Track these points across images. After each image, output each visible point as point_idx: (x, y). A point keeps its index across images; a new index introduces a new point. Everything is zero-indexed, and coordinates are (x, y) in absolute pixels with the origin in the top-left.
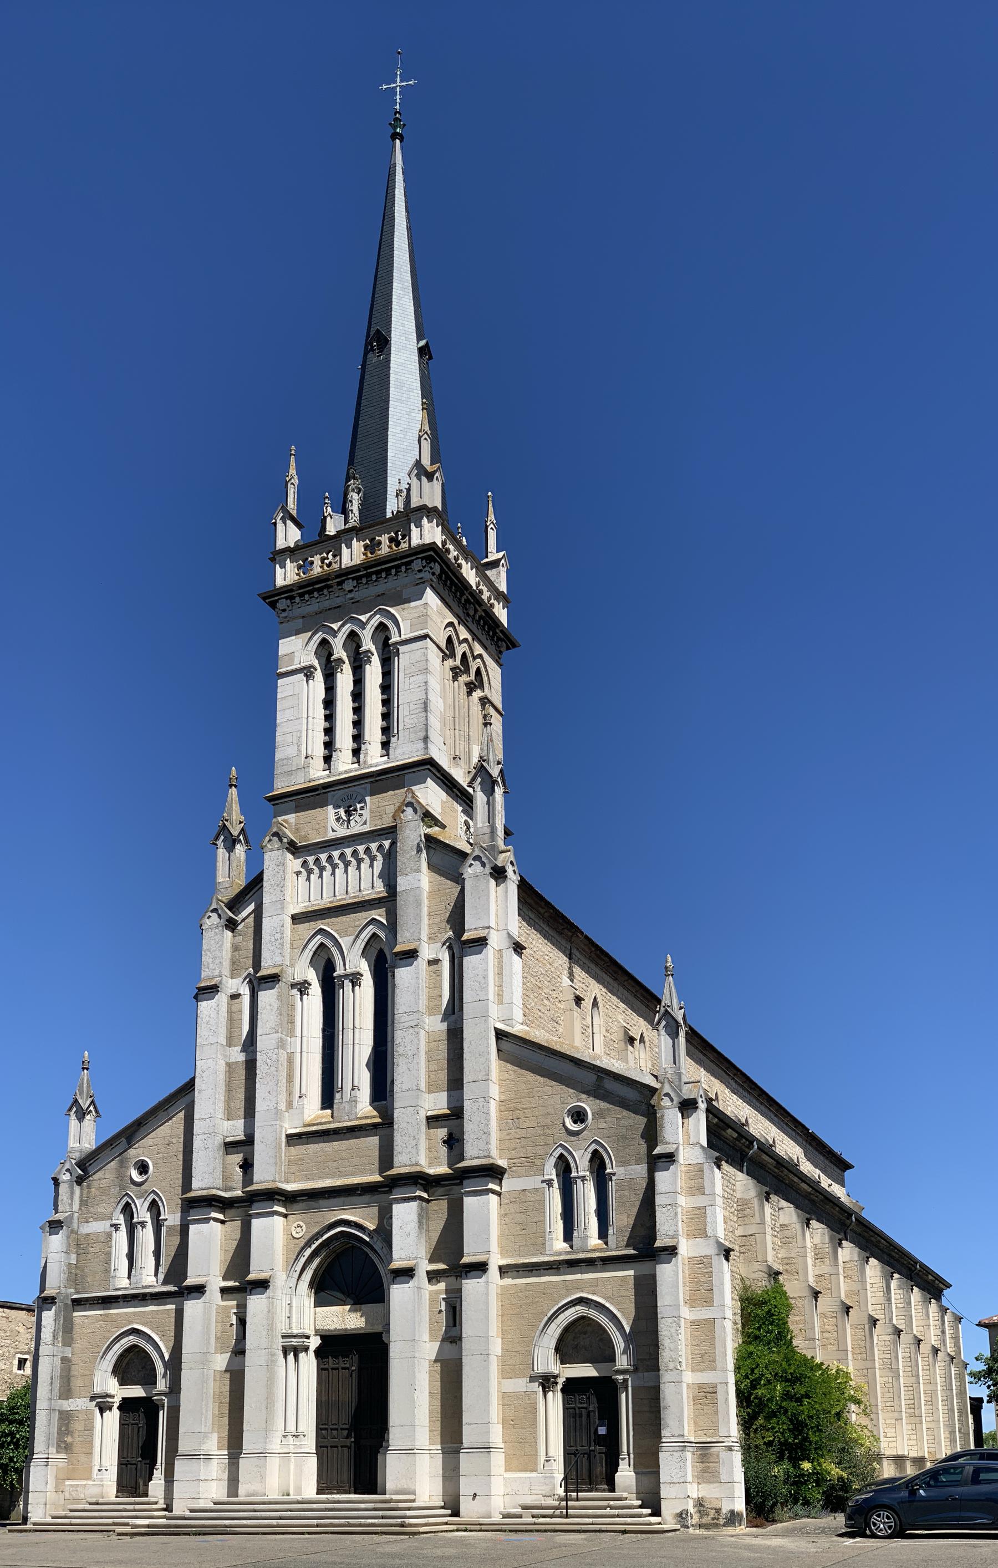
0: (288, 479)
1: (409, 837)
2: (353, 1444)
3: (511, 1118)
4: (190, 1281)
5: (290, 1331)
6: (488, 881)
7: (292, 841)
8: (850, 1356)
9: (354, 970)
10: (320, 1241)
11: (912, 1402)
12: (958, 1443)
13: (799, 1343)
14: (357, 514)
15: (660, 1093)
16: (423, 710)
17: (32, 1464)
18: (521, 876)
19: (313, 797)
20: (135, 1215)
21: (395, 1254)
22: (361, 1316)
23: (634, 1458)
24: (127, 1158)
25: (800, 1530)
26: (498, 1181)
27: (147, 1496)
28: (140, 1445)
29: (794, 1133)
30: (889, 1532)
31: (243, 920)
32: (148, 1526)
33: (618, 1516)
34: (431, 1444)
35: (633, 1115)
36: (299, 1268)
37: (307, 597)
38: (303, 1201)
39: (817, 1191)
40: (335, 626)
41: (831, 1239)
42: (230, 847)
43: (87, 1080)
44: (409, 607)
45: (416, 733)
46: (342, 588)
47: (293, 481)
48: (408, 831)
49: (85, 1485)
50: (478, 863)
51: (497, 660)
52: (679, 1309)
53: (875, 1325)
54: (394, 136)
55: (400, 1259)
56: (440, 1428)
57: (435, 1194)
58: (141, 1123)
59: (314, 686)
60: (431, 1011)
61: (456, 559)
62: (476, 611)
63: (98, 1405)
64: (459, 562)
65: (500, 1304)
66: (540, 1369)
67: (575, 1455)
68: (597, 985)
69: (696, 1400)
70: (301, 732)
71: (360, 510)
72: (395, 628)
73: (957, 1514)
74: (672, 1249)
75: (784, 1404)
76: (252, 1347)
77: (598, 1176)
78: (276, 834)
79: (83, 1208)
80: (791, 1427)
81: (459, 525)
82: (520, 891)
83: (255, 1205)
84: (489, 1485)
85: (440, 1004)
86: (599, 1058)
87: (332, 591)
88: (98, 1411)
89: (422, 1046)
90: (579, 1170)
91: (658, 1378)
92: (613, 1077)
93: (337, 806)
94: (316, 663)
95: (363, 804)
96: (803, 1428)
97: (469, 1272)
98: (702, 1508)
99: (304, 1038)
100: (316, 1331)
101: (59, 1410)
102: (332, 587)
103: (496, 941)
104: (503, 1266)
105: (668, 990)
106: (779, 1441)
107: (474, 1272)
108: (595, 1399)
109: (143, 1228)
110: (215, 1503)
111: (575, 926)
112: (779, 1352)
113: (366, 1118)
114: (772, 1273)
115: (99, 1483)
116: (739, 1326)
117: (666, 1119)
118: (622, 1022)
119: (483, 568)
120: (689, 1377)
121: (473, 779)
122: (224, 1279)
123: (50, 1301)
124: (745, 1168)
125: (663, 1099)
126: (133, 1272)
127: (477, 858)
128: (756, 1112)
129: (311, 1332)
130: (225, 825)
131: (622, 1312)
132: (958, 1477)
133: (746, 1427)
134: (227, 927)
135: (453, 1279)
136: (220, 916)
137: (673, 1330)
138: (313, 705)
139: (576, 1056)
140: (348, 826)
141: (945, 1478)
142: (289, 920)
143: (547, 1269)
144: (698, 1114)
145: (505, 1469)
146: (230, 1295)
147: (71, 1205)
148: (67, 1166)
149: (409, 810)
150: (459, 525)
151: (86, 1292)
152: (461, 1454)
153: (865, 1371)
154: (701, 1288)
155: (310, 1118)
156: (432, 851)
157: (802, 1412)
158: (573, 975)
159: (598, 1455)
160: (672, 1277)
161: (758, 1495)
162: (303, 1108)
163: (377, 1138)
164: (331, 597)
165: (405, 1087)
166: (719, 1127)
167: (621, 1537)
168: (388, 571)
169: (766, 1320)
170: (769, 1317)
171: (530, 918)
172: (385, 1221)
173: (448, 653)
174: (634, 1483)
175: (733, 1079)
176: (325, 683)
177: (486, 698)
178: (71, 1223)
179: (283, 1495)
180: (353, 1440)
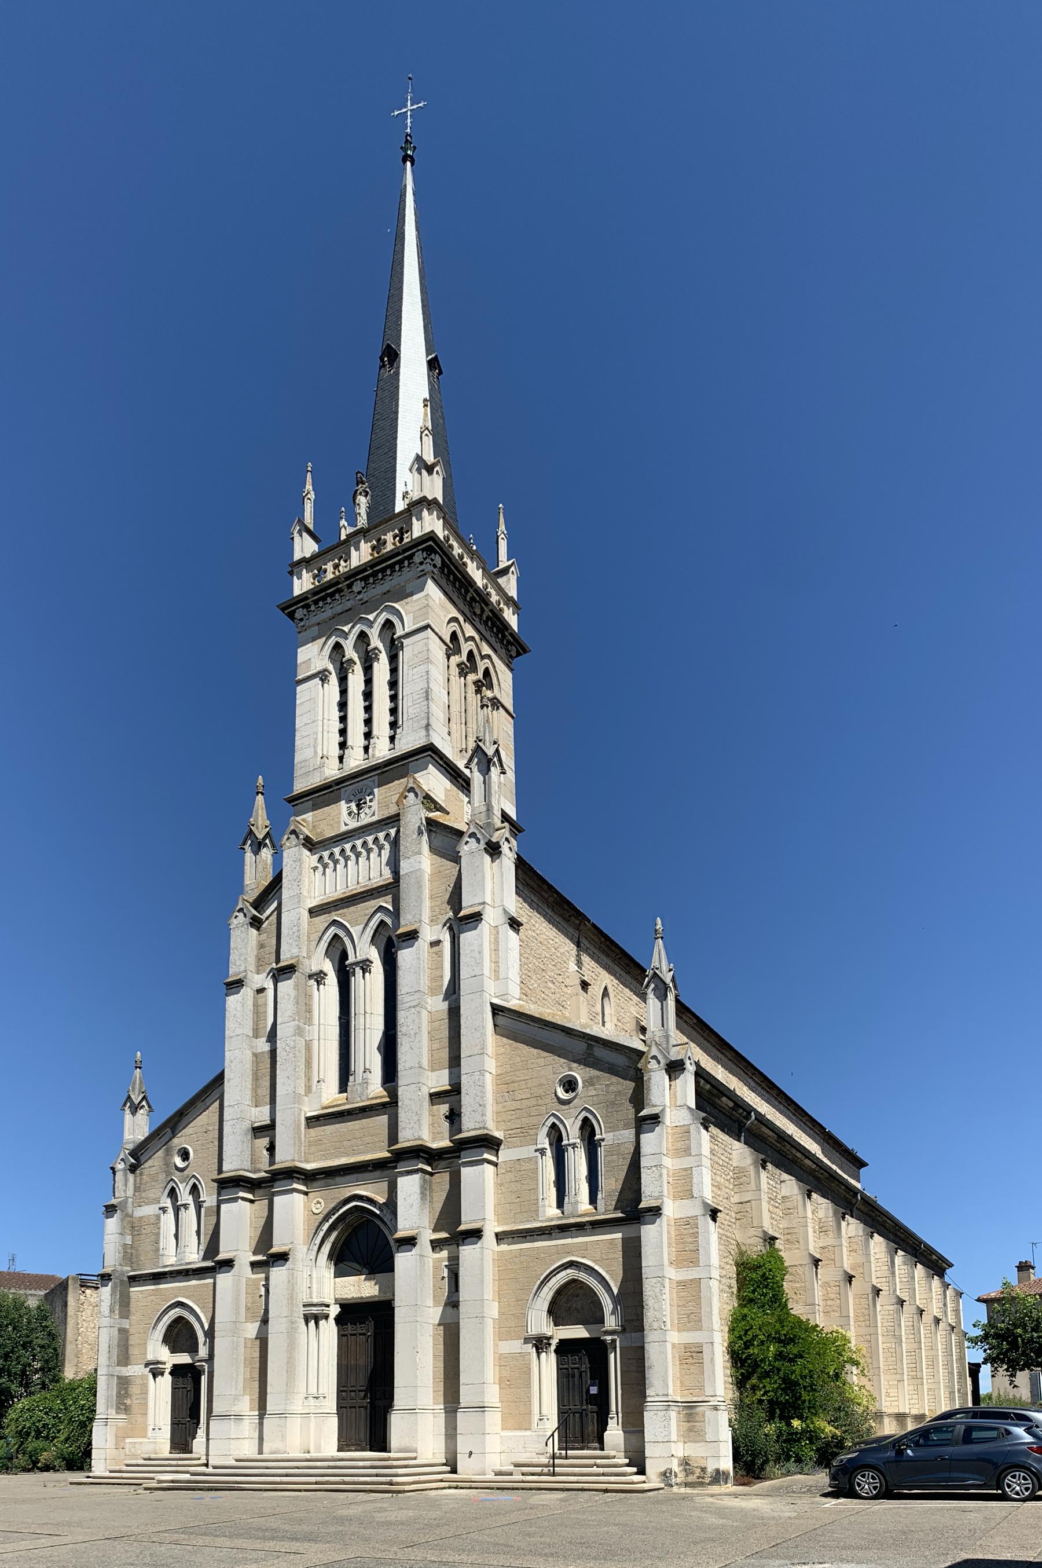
0: (304, 494)
2: (369, 1405)
3: (507, 1090)
4: (221, 1257)
5: (310, 1300)
7: (307, 836)
8: (852, 1323)
9: (364, 957)
10: (337, 1215)
11: (915, 1365)
12: (957, 1401)
13: (797, 1309)
14: (365, 517)
15: (647, 1056)
16: (424, 699)
17: (94, 1424)
18: (517, 854)
20: (179, 1199)
21: (400, 1226)
22: (375, 1284)
23: (623, 1417)
25: (787, 1488)
26: (495, 1152)
28: (189, 1407)
29: (812, 1132)
30: (874, 1492)
31: (267, 918)
32: (173, 1481)
33: (603, 1475)
35: (622, 1080)
36: (318, 1241)
37: (321, 604)
38: (322, 1178)
39: (821, 1168)
40: (346, 629)
41: (835, 1213)
42: (256, 852)
43: (140, 1078)
45: (418, 721)
46: (352, 591)
47: (309, 496)
48: (410, 816)
49: (141, 1443)
50: (473, 840)
51: (507, 664)
52: (663, 1270)
53: (878, 1295)
56: (442, 1389)
57: (439, 1168)
58: (183, 1114)
59: (329, 689)
60: (433, 992)
61: (461, 557)
62: (483, 611)
63: (151, 1371)
64: (464, 560)
65: (497, 1269)
68: (607, 975)
70: (317, 735)
71: (368, 514)
72: (400, 623)
73: (947, 1475)
74: (658, 1209)
78: (293, 832)
79: (136, 1194)
81: (471, 536)
82: (520, 871)
83: (278, 1183)
84: (483, 1443)
85: (441, 984)
87: (344, 595)
92: (603, 1044)
93: (349, 801)
94: (331, 668)
95: (372, 797)
97: (466, 1238)
98: (688, 1467)
100: (336, 1300)
101: (117, 1376)
103: (492, 917)
105: (657, 953)
107: (470, 1239)
108: (587, 1360)
109: (186, 1209)
110: (237, 1460)
111: (582, 913)
112: (773, 1314)
113: (376, 1098)
114: (767, 1238)
116: (735, 1290)
117: (653, 1081)
118: (635, 1013)
119: (489, 561)
120: (674, 1337)
121: (470, 760)
122: (255, 1253)
124: (742, 1138)
125: (650, 1062)
127: (473, 835)
128: (774, 1110)
130: (251, 829)
131: (610, 1274)
132: (949, 1436)
134: (252, 925)
136: (245, 915)
137: (657, 1290)
138: (329, 708)
139: (567, 1025)
140: (358, 819)
141: (936, 1437)
142: (306, 914)
143: (540, 1235)
144: (685, 1076)
146: (260, 1268)
147: (125, 1191)
148: (122, 1156)
149: (411, 795)
150: (471, 536)
151: (140, 1270)
153: (868, 1337)
154: (687, 1249)
155: (328, 1102)
157: (794, 1372)
158: (581, 963)
159: (590, 1414)
161: (747, 1454)
162: (321, 1092)
163: (386, 1117)
164: (343, 601)
165: (408, 1066)
168: (392, 567)
169: (761, 1283)
171: (532, 901)
173: (452, 646)
175: (751, 1078)
176: (340, 686)
177: (495, 698)
178: (126, 1207)
179: (304, 1453)
180: (369, 1400)
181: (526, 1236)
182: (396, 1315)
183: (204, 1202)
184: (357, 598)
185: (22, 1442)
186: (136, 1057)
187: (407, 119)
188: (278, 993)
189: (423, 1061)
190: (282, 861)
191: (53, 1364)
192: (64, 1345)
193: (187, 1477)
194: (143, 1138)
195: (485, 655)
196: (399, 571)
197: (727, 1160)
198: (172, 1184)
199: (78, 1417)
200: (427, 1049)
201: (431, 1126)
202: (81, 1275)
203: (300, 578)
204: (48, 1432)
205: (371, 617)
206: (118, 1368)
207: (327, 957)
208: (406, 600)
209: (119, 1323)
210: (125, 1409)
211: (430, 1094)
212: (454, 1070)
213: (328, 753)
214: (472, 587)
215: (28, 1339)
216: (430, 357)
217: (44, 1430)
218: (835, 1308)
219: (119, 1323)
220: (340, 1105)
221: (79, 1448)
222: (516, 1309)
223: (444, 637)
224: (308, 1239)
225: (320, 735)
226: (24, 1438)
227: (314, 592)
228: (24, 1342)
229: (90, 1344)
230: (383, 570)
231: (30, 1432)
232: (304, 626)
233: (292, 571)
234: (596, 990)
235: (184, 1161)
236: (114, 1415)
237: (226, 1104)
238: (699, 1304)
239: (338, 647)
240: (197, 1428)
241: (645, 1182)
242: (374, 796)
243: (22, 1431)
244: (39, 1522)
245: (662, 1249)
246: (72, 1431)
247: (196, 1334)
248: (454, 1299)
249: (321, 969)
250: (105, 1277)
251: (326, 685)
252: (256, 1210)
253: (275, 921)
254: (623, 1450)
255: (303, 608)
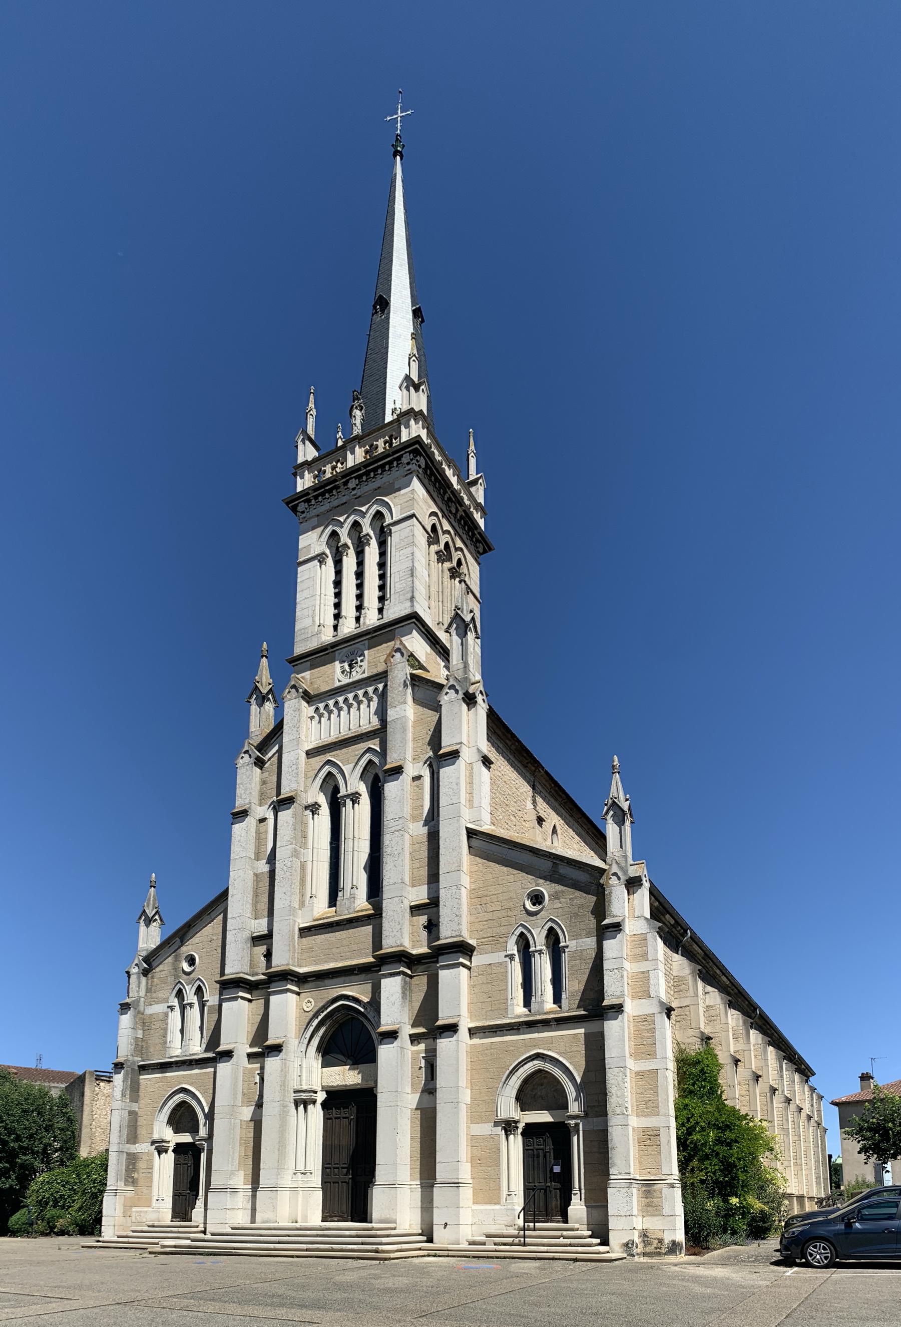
1: (397, 676)
2: (350, 1180)
4: (222, 1048)
5: (300, 1087)
6: (461, 705)
7: (306, 690)
9: (354, 791)
10: (325, 1013)
14: (360, 427)
15: (608, 873)
17: (105, 1194)
18: (489, 706)
19: (324, 657)
20: (185, 999)
21: (383, 1021)
22: (358, 1074)
24: (180, 954)
26: (468, 958)
27: (190, 1220)
30: (826, 1262)
31: (269, 759)
32: (175, 1247)
33: (570, 1245)
34: (411, 1180)
35: (584, 895)
36: (308, 1035)
37: (320, 499)
40: (342, 519)
41: (745, 1022)
42: (261, 704)
43: (154, 896)
44: (399, 495)
45: (404, 595)
46: (348, 488)
47: (311, 412)
49: (146, 1212)
50: (452, 691)
52: (625, 1060)
54: (396, 153)
55: (387, 1025)
56: (419, 1167)
57: (418, 971)
59: (326, 570)
60: (415, 819)
62: (457, 510)
63: (157, 1149)
65: (469, 1060)
66: (503, 1115)
67: (533, 1190)
68: (556, 816)
69: (641, 1143)
70: (315, 607)
71: (362, 425)
72: (389, 513)
74: (620, 1006)
75: (716, 1148)
76: (268, 1101)
77: (553, 951)
78: (294, 687)
80: (722, 1167)
82: (489, 719)
83: (273, 984)
84: (458, 1216)
86: (555, 848)
87: (340, 492)
88: (157, 1153)
89: (406, 846)
90: (537, 945)
91: (606, 1122)
92: (567, 863)
93: (342, 662)
94: (328, 552)
95: (363, 658)
96: (732, 1168)
98: (646, 1239)
99: (315, 850)
100: (323, 1087)
101: (127, 1153)
102: (339, 487)
103: (468, 755)
104: (471, 1028)
106: (711, 1179)
107: (447, 1033)
109: (191, 1008)
110: (232, 1228)
113: (362, 911)
115: (156, 1210)
119: (462, 473)
120: (634, 1122)
122: (251, 1046)
123: (119, 1067)
124: (680, 952)
125: (611, 878)
126: (183, 1043)
127: (452, 687)
129: (318, 1088)
130: (256, 686)
131: (574, 1065)
133: (683, 1167)
134: (256, 764)
135: (432, 1040)
136: (250, 756)
138: (325, 585)
141: (867, 1211)
142: (304, 755)
143: (509, 1030)
144: (643, 891)
145: (473, 1202)
146: (255, 1059)
147: (138, 992)
148: (136, 962)
149: (398, 655)
151: (149, 1060)
152: (434, 1189)
154: (645, 1042)
156: (417, 688)
157: (732, 1155)
159: (553, 1191)
160: (619, 1032)
161: (695, 1227)
165: (392, 881)
166: (659, 911)
167: (572, 1265)
170: (702, 1075)
171: (498, 746)
172: (377, 994)
174: (585, 1216)
176: (335, 568)
178: (138, 1005)
179: (293, 1222)
180: (351, 1177)
181: (496, 1032)
182: (378, 1100)
183: (208, 1001)
184: (352, 493)
185: (41, 1210)
186: (151, 877)
187: (397, 124)
188: (278, 821)
189: (406, 877)
190: (284, 710)
191: (70, 1145)
192: (80, 1129)
193: (188, 1242)
194: (155, 947)
195: (459, 547)
196: (389, 470)
197: (669, 970)
198: (179, 986)
199: (91, 1189)
200: (408, 867)
201: (411, 935)
202: (96, 1071)
203: (302, 477)
204: (64, 1202)
205: (364, 509)
206: (128, 1146)
207: (322, 792)
208: (394, 495)
209: (128, 1106)
210: (133, 1182)
211: (410, 906)
212: (432, 886)
213: (324, 622)
214: (449, 488)
215: (50, 1123)
216: (414, 308)
217: (61, 1201)
218: (744, 1103)
219: (128, 1106)
220: (329, 917)
221: (90, 1216)
222: (487, 1096)
223: (426, 527)
224: (300, 1034)
225: (318, 607)
226: (43, 1207)
227: (314, 488)
228: (46, 1125)
229: (102, 1129)
230: (375, 470)
231: (49, 1202)
232: (305, 518)
233: (296, 472)
234: (548, 826)
235: (190, 966)
236: (122, 1187)
237: (229, 916)
238: (656, 1092)
239: (334, 534)
240: (196, 1199)
241: (608, 982)
242: (364, 656)
243: (41, 1200)
244: (52, 1284)
245: (624, 1042)
246: (85, 1201)
247: (197, 1117)
248: (431, 1086)
249: (316, 801)
250: (118, 1065)
251: (323, 566)
252: (253, 1008)
253: (276, 762)
254: (586, 1223)
255: (305, 503)
